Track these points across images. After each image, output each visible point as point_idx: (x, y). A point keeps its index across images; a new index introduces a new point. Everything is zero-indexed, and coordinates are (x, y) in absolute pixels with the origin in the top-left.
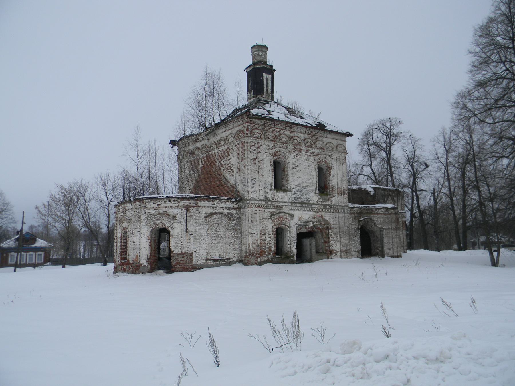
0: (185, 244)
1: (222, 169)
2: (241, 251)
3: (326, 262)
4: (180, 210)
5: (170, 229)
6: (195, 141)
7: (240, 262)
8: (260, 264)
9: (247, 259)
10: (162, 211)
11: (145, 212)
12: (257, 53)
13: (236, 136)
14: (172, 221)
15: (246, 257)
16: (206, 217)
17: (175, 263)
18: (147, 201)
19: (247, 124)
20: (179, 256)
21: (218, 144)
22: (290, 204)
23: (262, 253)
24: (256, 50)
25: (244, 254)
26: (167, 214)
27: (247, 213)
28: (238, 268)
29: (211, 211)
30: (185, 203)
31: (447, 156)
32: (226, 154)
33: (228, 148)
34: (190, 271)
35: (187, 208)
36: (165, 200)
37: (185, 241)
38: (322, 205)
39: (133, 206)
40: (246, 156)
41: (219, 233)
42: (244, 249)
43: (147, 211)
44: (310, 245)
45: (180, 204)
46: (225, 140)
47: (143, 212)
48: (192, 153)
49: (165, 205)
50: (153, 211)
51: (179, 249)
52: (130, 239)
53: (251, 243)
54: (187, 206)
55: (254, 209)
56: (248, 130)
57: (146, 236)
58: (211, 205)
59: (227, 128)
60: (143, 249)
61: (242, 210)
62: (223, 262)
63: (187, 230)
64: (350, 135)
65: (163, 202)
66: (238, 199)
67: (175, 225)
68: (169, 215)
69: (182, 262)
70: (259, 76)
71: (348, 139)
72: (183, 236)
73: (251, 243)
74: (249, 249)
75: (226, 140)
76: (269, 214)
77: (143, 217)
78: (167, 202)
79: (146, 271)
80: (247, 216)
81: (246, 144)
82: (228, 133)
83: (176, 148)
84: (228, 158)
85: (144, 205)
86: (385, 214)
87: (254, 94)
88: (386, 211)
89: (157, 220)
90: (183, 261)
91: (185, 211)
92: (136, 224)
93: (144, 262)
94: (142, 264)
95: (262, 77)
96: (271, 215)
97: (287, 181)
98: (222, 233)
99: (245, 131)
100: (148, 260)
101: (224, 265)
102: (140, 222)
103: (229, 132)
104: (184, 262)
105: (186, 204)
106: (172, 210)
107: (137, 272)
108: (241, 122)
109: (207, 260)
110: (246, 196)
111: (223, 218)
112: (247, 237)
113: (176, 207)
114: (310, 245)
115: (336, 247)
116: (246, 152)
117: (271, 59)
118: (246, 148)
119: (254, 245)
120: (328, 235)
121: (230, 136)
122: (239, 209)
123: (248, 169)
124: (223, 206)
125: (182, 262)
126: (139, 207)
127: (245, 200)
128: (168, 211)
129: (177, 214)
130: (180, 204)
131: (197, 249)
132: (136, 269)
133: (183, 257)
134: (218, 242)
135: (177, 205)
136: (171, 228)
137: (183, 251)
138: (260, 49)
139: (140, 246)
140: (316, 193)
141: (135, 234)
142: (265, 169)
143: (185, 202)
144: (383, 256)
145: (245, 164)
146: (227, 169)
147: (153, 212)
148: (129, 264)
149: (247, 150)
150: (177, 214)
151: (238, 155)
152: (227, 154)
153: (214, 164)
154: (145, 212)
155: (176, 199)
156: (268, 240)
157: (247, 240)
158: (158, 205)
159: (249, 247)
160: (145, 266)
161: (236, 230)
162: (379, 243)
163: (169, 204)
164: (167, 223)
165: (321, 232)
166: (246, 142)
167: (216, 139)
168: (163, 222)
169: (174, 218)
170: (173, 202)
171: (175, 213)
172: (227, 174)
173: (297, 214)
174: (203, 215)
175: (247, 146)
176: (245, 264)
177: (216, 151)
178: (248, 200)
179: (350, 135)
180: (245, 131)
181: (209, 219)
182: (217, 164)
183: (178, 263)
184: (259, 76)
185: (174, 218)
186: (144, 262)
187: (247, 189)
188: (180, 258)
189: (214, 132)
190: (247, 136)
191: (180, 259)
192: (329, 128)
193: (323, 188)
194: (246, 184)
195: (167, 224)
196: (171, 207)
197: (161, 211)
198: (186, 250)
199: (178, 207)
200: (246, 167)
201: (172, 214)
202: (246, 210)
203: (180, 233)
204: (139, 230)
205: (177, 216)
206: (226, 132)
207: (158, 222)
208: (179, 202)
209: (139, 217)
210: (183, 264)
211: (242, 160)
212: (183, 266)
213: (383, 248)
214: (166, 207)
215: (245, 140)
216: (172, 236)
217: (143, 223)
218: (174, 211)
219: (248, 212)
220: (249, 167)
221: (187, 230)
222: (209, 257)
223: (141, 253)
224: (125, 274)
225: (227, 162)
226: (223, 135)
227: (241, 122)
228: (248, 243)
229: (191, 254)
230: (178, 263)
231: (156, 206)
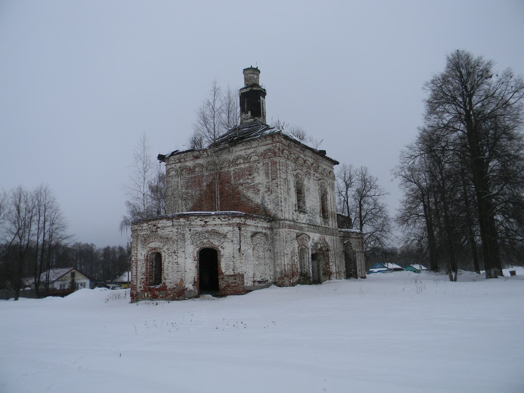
0: (238, 265)
1: (240, 188)
2: (275, 272)
3: (329, 283)
4: (231, 228)
5: (220, 248)
6: (197, 158)
7: (275, 283)
8: (293, 285)
9: (281, 281)
10: (210, 229)
11: (190, 230)
12: (252, 75)
13: (264, 155)
14: (222, 240)
15: (282, 278)
16: (252, 236)
17: (224, 285)
18: (193, 218)
19: (278, 144)
20: (230, 278)
21: (234, 162)
22: (306, 226)
23: (293, 275)
24: (251, 72)
25: (278, 275)
26: (217, 233)
27: (281, 233)
28: (274, 290)
29: (254, 230)
30: (237, 220)
31: (347, 190)
32: (247, 173)
33: (250, 167)
34: (242, 294)
35: (239, 226)
36: (214, 217)
37: (238, 261)
38: (324, 227)
39: (175, 223)
40: (279, 176)
41: (259, 254)
42: (278, 269)
43: (192, 229)
44: (318, 266)
45: (230, 222)
46: (244, 158)
47: (188, 229)
48: (191, 170)
49: (214, 223)
50: (200, 229)
51: (231, 270)
52: (167, 260)
53: (286, 263)
54: (239, 223)
55: (287, 230)
56: (279, 149)
57: (192, 256)
58: (254, 224)
59: (248, 147)
60: (188, 271)
61: (275, 230)
62: (263, 284)
63: (240, 249)
64: (337, 163)
65: (212, 219)
66: (272, 219)
67: (226, 245)
68: (220, 234)
69: (233, 285)
70: (252, 98)
71: (335, 167)
72: (235, 256)
73: (286, 263)
74: (285, 270)
75: (246, 159)
76: (294, 236)
77: (188, 236)
78: (217, 219)
79: (192, 295)
80: (281, 236)
81: (278, 164)
82: (249, 152)
83: (163, 163)
84: (250, 177)
85: (189, 223)
86: (356, 238)
87: (251, 115)
88: (357, 235)
89: (204, 239)
90: (235, 283)
91: (237, 229)
92: (180, 243)
93: (189, 286)
94: (187, 289)
95: (260, 99)
96: (297, 236)
97: (304, 203)
98: (261, 254)
99: (277, 151)
100: (195, 284)
101: (262, 288)
102: (184, 240)
103: (252, 150)
104: (236, 284)
105: (238, 222)
106: (221, 228)
107: (181, 298)
108: (270, 142)
109: (254, 282)
110: (280, 215)
111: (263, 238)
112: (282, 257)
113: (226, 224)
114: (318, 266)
115: (333, 269)
116: (278, 172)
117: (263, 82)
118: (278, 167)
119: (289, 266)
120: (328, 256)
121: (253, 155)
122: (271, 229)
123: (281, 189)
124: (262, 225)
125: (233, 285)
126: (183, 224)
127: (279, 220)
128: (217, 228)
129: (228, 233)
130: (230, 222)
131: (247, 270)
132: (179, 294)
133: (235, 279)
134: (260, 263)
135: (227, 223)
136: (221, 247)
137: (236, 272)
138: (252, 73)
139: (183, 266)
140: (320, 216)
141: (179, 255)
142: (291, 190)
143: (237, 219)
144: (357, 278)
145: (277, 183)
146: (248, 188)
147: (200, 230)
148: (165, 290)
149: (280, 169)
150: (228, 233)
151: (267, 174)
152: (250, 171)
153: (228, 182)
154: (190, 230)
155: (226, 216)
156: (296, 260)
157: (283, 261)
158: (206, 222)
159: (285, 268)
160: (191, 291)
161: (270, 250)
162: (353, 265)
163: (218, 221)
164: (216, 242)
165: (323, 254)
166: (278, 161)
167: (231, 157)
168: (212, 241)
169: (225, 236)
170: (223, 220)
171: (225, 231)
172: (250, 194)
173: (312, 235)
174: (250, 234)
175: (280, 166)
176: (280, 286)
177: (232, 169)
178: (282, 220)
179: (337, 163)
180: (277, 151)
181: (254, 238)
182: (233, 182)
183: (228, 286)
184: (252, 98)
185: (225, 236)
186: (189, 286)
187: (280, 209)
188: (231, 280)
189: (228, 150)
190: (279, 156)
191: (230, 281)
192: (327, 155)
193: (324, 211)
194: (280, 204)
195: (217, 244)
196: (221, 225)
197: (210, 228)
198: (239, 271)
199: (229, 225)
200: (279, 186)
201: (222, 232)
202: (281, 230)
203: (232, 253)
204: (183, 250)
205: (228, 235)
206: (247, 151)
207: (205, 241)
208: (229, 220)
209: (184, 235)
210: (235, 286)
211: (273, 179)
212: (235, 288)
213: (356, 269)
214: (215, 225)
215: (277, 159)
216: (223, 256)
217: (188, 242)
218: (225, 229)
219: (283, 232)
220: (282, 187)
221: (240, 249)
222: (255, 279)
223: (186, 276)
224: (155, 302)
225: (249, 181)
226: (243, 153)
227: (270, 142)
228: (283, 264)
229: (242, 276)
230: (228, 286)
231: (203, 223)
